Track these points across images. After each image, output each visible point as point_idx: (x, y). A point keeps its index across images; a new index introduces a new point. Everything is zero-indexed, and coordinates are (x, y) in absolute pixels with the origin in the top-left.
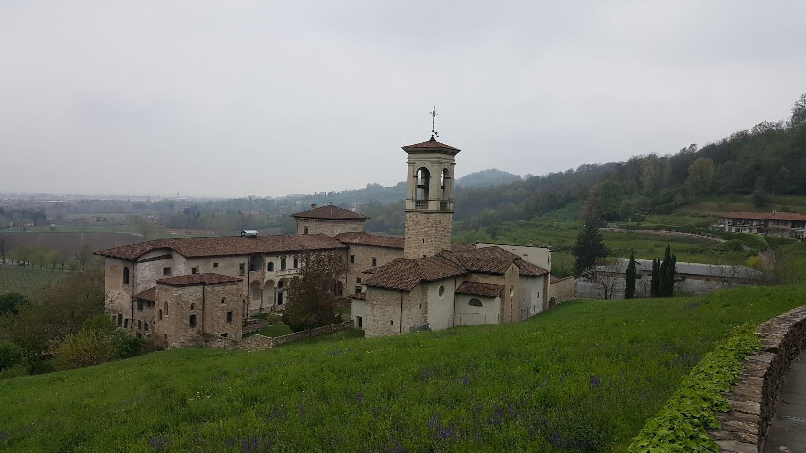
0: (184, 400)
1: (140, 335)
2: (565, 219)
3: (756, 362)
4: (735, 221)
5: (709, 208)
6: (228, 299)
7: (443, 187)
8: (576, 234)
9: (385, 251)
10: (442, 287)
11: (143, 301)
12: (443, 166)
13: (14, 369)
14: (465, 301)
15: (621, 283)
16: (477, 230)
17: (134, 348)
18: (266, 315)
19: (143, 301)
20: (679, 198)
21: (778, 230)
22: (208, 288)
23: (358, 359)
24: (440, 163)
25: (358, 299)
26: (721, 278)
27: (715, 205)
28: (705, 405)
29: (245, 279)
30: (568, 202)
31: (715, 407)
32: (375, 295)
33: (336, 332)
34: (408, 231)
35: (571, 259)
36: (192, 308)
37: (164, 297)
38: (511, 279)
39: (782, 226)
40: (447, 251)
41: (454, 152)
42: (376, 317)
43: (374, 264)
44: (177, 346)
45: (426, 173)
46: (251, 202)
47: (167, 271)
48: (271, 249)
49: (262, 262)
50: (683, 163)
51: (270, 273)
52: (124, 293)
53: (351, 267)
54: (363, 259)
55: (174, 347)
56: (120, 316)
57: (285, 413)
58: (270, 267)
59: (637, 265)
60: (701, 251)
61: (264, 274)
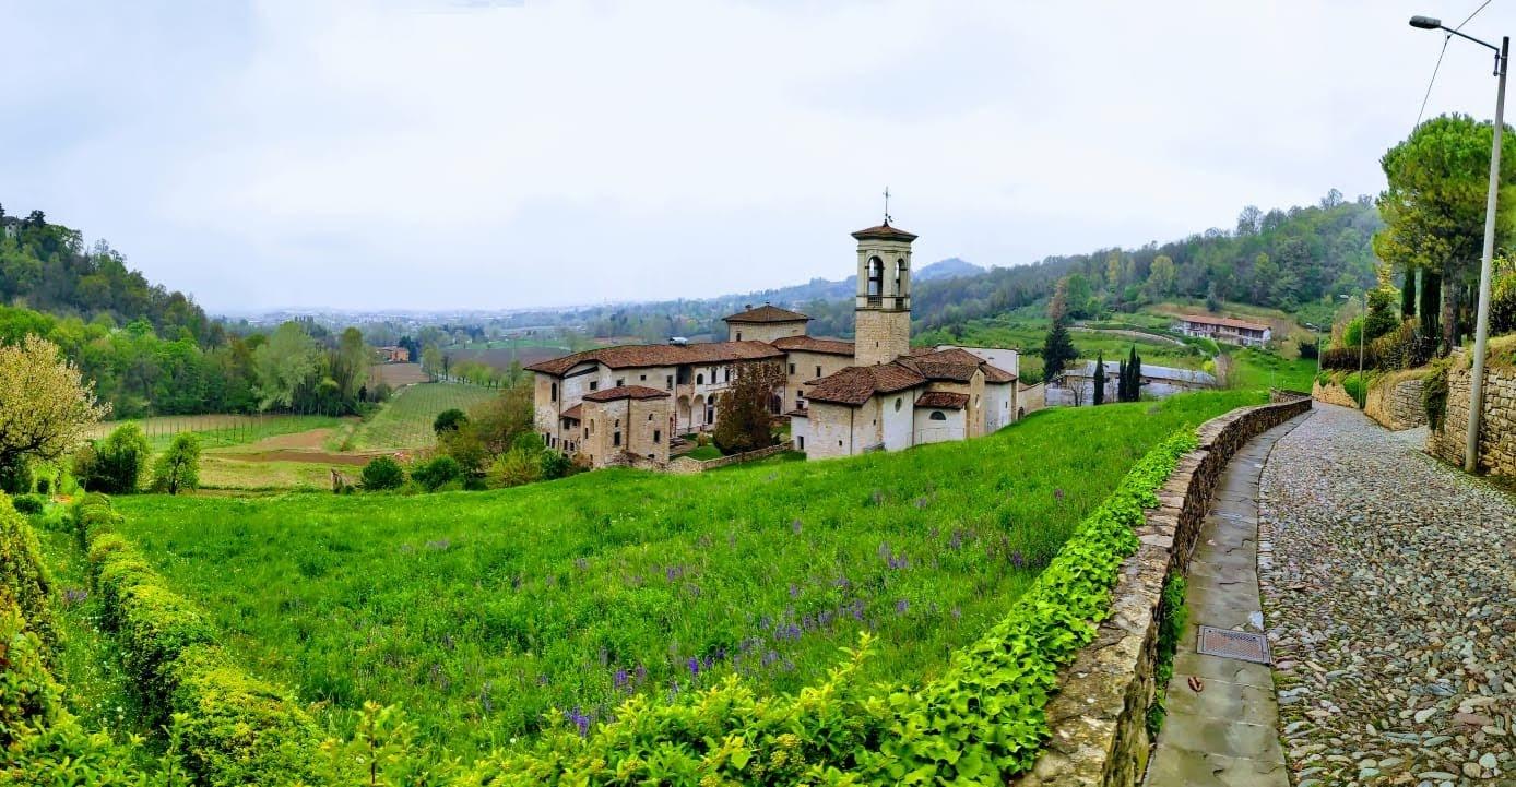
0: (608, 522)
1: (565, 456)
2: (1033, 317)
3: (1189, 459)
4: (1193, 325)
5: (1169, 309)
6: (655, 417)
7: (898, 281)
8: (1044, 334)
9: (832, 358)
10: (899, 400)
11: (569, 420)
12: (898, 256)
13: (452, 483)
14: (926, 414)
15: (1090, 388)
16: (939, 331)
17: (560, 469)
18: (695, 435)
19: (569, 420)
20: (1142, 297)
21: (1227, 337)
22: (634, 403)
23: (797, 483)
24: (895, 252)
25: (799, 416)
26: (1180, 383)
27: (1175, 306)
28: (1135, 502)
29: (673, 393)
30: (1035, 299)
31: (1144, 505)
32: (818, 411)
33: (772, 455)
34: (859, 334)
35: (1039, 363)
37: (591, 413)
38: (976, 387)
39: (1231, 333)
41: (909, 238)
42: (824, 438)
43: (819, 374)
44: (603, 467)
46: (680, 306)
47: (593, 385)
50: (1143, 263)
51: (701, 387)
52: (552, 411)
53: (791, 379)
54: (805, 368)
55: (598, 468)
56: (548, 435)
57: (714, 541)
58: (700, 380)
59: (1104, 368)
60: (1164, 354)
61: (693, 388)
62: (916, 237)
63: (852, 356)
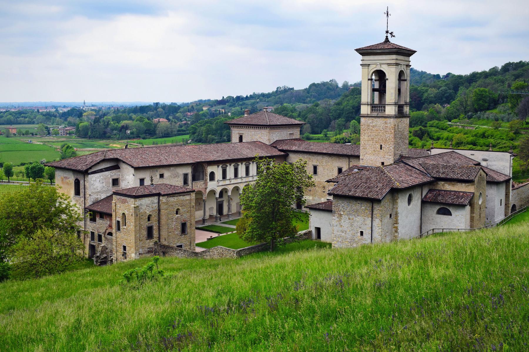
6: (181, 210)
11: (95, 213)
12: (400, 68)
22: (163, 199)
24: (397, 64)
32: (340, 206)
36: (149, 220)
40: (405, 157)
42: (341, 229)
45: (381, 75)
47: (115, 182)
48: (212, 158)
49: (204, 172)
58: (212, 176)
61: (206, 184)
62: (415, 52)
63: (358, 157)
